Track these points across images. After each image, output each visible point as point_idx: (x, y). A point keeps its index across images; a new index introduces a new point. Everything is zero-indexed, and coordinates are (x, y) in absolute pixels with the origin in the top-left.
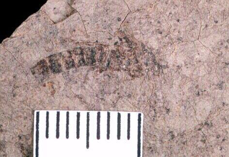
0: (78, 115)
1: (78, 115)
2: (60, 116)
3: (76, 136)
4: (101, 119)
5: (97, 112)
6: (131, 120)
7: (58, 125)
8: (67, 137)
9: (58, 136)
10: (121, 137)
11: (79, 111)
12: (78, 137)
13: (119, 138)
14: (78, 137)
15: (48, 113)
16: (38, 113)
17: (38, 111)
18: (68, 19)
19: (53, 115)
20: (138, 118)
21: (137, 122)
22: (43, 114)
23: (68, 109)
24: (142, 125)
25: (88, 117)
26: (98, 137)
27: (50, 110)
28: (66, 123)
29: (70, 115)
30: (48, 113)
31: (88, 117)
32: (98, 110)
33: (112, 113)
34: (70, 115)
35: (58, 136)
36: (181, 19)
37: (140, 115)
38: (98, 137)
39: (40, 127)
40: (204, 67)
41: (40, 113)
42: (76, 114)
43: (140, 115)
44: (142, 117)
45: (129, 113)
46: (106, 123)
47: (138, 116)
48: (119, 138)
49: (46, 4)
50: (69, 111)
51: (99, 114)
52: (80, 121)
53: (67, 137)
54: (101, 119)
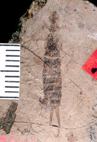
1: (18, 66)
3: (7, 65)
7: (13, 56)
8: (7, 61)
9: (7, 56)
10: (6, 88)
11: (20, 66)
12: (6, 66)
13: (6, 87)
14: (6, 66)
15: (19, 51)
16: (19, 46)
19: (18, 74)
23: (20, 93)
24: (14, 99)
25: (17, 61)
26: (6, 77)
30: (19, 51)
31: (17, 61)
34: (18, 62)
35: (7, 56)
36: (75, 9)
38: (6, 77)
39: (12, 46)
40: (72, 105)
41: (18, 67)
44: (17, 99)
48: (6, 87)
49: (61, 65)
50: (20, 51)
53: (7, 61)
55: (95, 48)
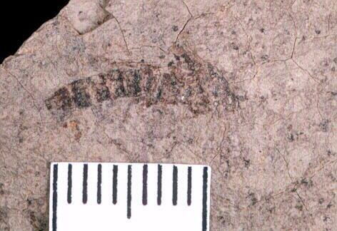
0: (115, 169)
1: (115, 169)
2: (89, 170)
3: (112, 200)
4: (149, 175)
5: (143, 164)
6: (192, 176)
7: (85, 184)
8: (99, 201)
9: (85, 200)
10: (178, 202)
11: (116, 164)
12: (115, 201)
13: (175, 202)
14: (115, 201)
15: (70, 167)
16: (56, 167)
17: (56, 163)
18: (99, 28)
19: (78, 169)
20: (202, 174)
21: (202, 179)
22: (63, 168)
23: (100, 160)
24: (209, 184)
25: (130, 172)
26: (145, 202)
27: (74, 162)
28: (96, 181)
29: (103, 169)
30: (70, 167)
31: (130, 172)
32: (144, 162)
33: (164, 166)
34: (102, 169)
35: (85, 200)
36: (266, 28)
37: (205, 169)
38: (145, 202)
39: (58, 186)
40: (300, 99)
41: (59, 167)
42: (112, 168)
43: (205, 169)
44: (209, 171)
45: (190, 166)
46: (157, 181)
47: (202, 171)
48: (175, 202)
49: (68, 5)
50: (102, 164)
51: (145, 168)
52: (118, 178)
53: (99, 201)
54: (149, 175)
55: (336, 57)
